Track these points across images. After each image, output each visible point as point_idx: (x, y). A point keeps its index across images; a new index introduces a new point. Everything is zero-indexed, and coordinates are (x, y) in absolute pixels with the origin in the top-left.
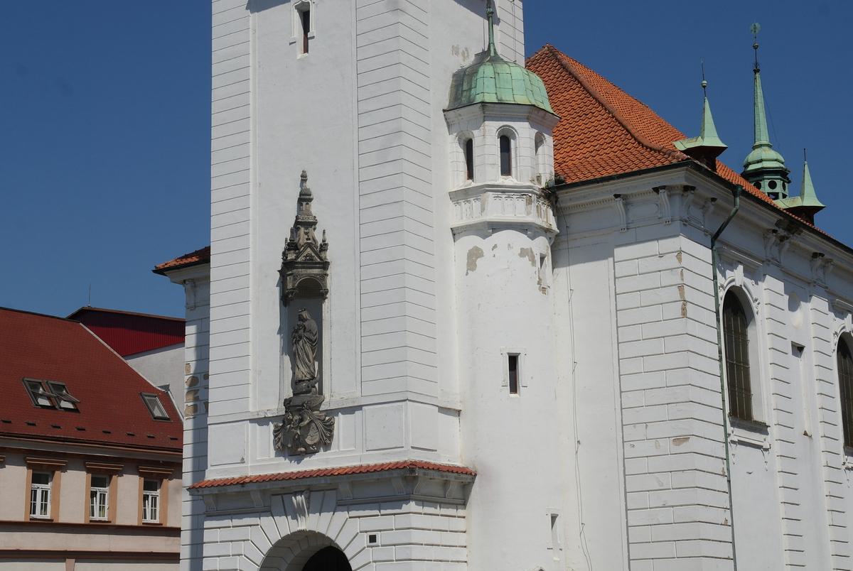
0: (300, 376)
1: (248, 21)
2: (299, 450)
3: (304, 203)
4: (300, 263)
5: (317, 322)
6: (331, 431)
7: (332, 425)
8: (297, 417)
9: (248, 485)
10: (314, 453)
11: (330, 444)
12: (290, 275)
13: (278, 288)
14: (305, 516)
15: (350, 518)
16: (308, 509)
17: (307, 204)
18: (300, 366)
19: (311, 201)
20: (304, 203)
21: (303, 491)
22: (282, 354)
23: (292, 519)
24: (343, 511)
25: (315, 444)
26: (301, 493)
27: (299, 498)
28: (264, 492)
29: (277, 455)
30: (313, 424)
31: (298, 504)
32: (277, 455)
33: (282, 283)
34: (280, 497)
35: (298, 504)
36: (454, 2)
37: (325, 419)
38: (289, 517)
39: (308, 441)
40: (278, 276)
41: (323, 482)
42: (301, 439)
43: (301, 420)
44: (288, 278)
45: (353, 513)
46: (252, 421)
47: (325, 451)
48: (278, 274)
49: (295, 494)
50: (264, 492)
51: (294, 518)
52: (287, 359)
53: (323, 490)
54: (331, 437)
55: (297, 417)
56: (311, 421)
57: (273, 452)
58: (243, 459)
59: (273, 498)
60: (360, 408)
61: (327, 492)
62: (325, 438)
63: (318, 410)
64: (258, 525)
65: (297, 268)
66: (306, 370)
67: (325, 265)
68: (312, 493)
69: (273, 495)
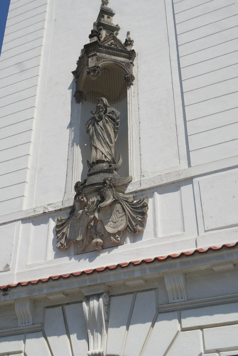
0: (96, 155)
1: (36, 90)
2: (94, 241)
3: (106, 16)
4: (106, 47)
5: (100, 163)
6: (144, 214)
7: (145, 206)
8: (94, 199)
9: (14, 290)
10: (116, 245)
11: (141, 233)
12: (93, 56)
13: (71, 90)
14: (101, 334)
15: (183, 330)
16: (107, 321)
17: (108, 18)
18: (99, 146)
19: (112, 16)
20: (106, 16)
21: (103, 293)
22: (73, 145)
23: (79, 338)
24: (170, 319)
25: (119, 232)
26: (98, 296)
27: (94, 303)
28: (35, 302)
29: (57, 256)
30: (118, 206)
31: (92, 313)
32: (57, 256)
33: (82, 62)
34: (60, 307)
35: (92, 313)
36: (27, 355)
37: (133, 202)
38: (74, 337)
39: (109, 229)
40: (71, 78)
41: (137, 274)
42: (99, 226)
43: (103, 199)
44: (90, 59)
45: (188, 322)
46: (24, 220)
47: (133, 241)
48: (72, 75)
49: (88, 299)
50: (35, 302)
51: (84, 336)
52: (78, 150)
53: (132, 293)
54: (142, 224)
55: (94, 199)
56: (116, 202)
57: (51, 253)
58: (7, 266)
59: (48, 310)
60: (189, 180)
61: (138, 294)
62: (134, 224)
63: (124, 193)
64: (20, 352)
65: (100, 52)
66: (107, 150)
67: (131, 55)
68: (113, 298)
69: (47, 307)
